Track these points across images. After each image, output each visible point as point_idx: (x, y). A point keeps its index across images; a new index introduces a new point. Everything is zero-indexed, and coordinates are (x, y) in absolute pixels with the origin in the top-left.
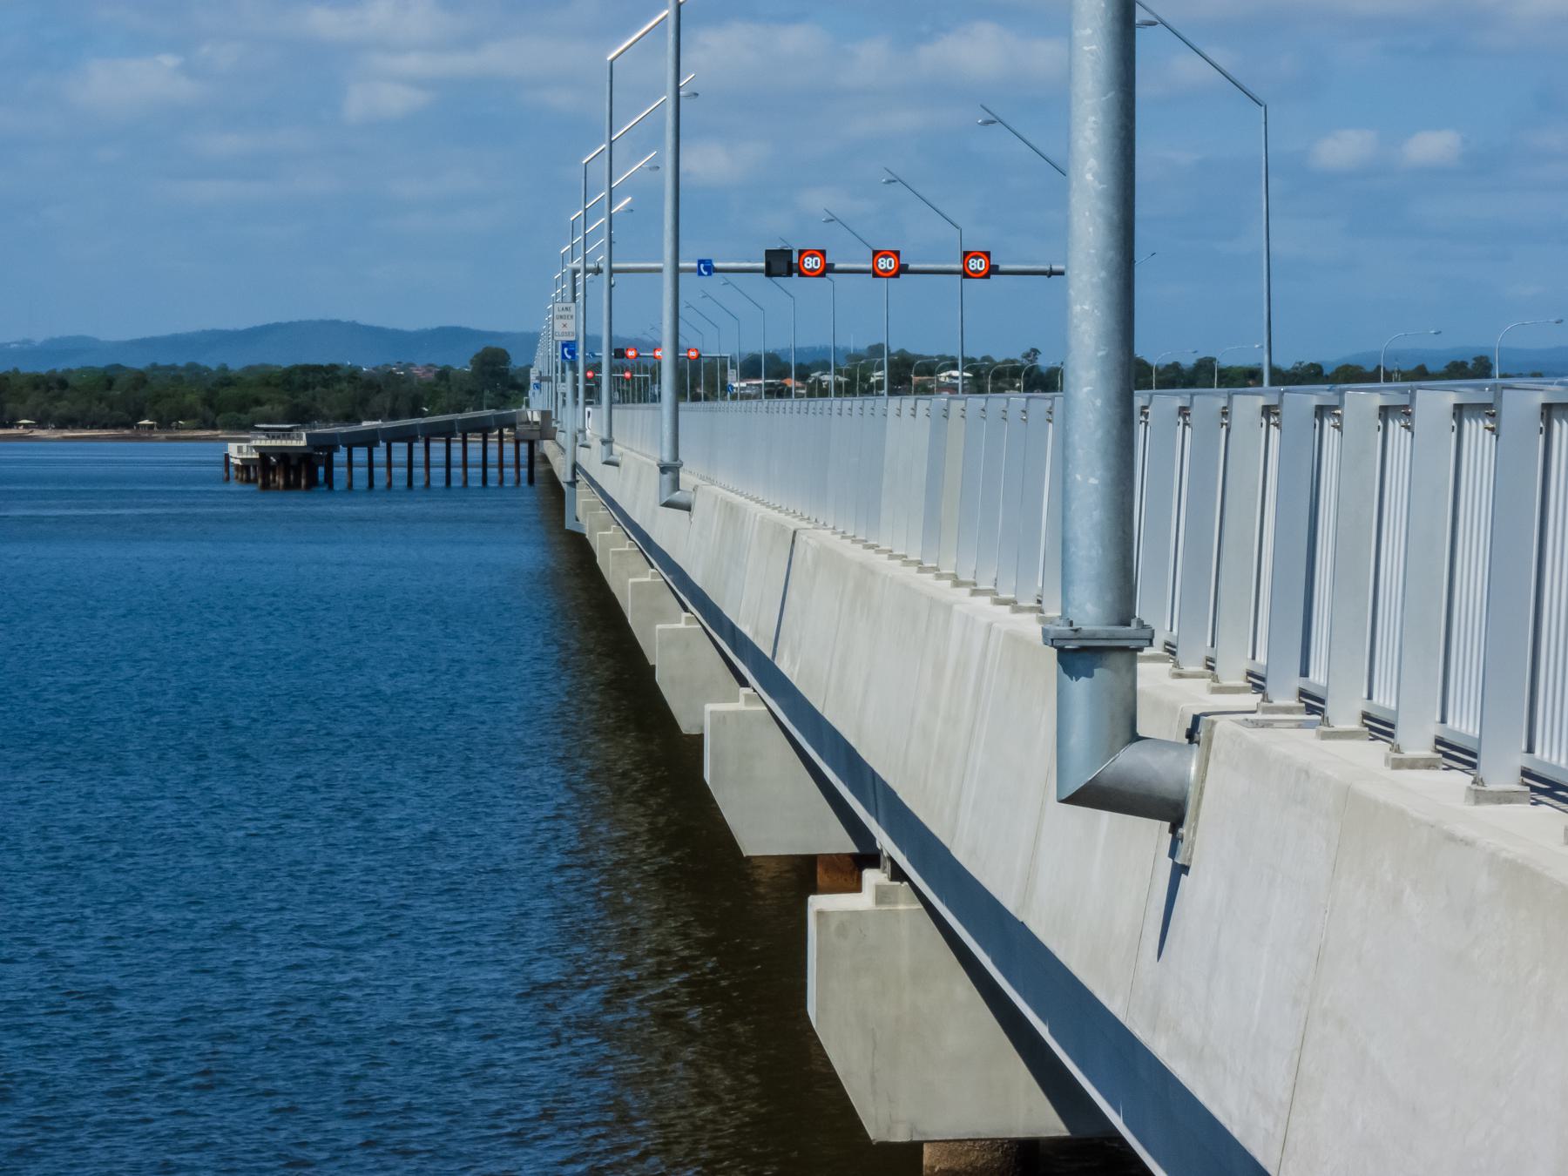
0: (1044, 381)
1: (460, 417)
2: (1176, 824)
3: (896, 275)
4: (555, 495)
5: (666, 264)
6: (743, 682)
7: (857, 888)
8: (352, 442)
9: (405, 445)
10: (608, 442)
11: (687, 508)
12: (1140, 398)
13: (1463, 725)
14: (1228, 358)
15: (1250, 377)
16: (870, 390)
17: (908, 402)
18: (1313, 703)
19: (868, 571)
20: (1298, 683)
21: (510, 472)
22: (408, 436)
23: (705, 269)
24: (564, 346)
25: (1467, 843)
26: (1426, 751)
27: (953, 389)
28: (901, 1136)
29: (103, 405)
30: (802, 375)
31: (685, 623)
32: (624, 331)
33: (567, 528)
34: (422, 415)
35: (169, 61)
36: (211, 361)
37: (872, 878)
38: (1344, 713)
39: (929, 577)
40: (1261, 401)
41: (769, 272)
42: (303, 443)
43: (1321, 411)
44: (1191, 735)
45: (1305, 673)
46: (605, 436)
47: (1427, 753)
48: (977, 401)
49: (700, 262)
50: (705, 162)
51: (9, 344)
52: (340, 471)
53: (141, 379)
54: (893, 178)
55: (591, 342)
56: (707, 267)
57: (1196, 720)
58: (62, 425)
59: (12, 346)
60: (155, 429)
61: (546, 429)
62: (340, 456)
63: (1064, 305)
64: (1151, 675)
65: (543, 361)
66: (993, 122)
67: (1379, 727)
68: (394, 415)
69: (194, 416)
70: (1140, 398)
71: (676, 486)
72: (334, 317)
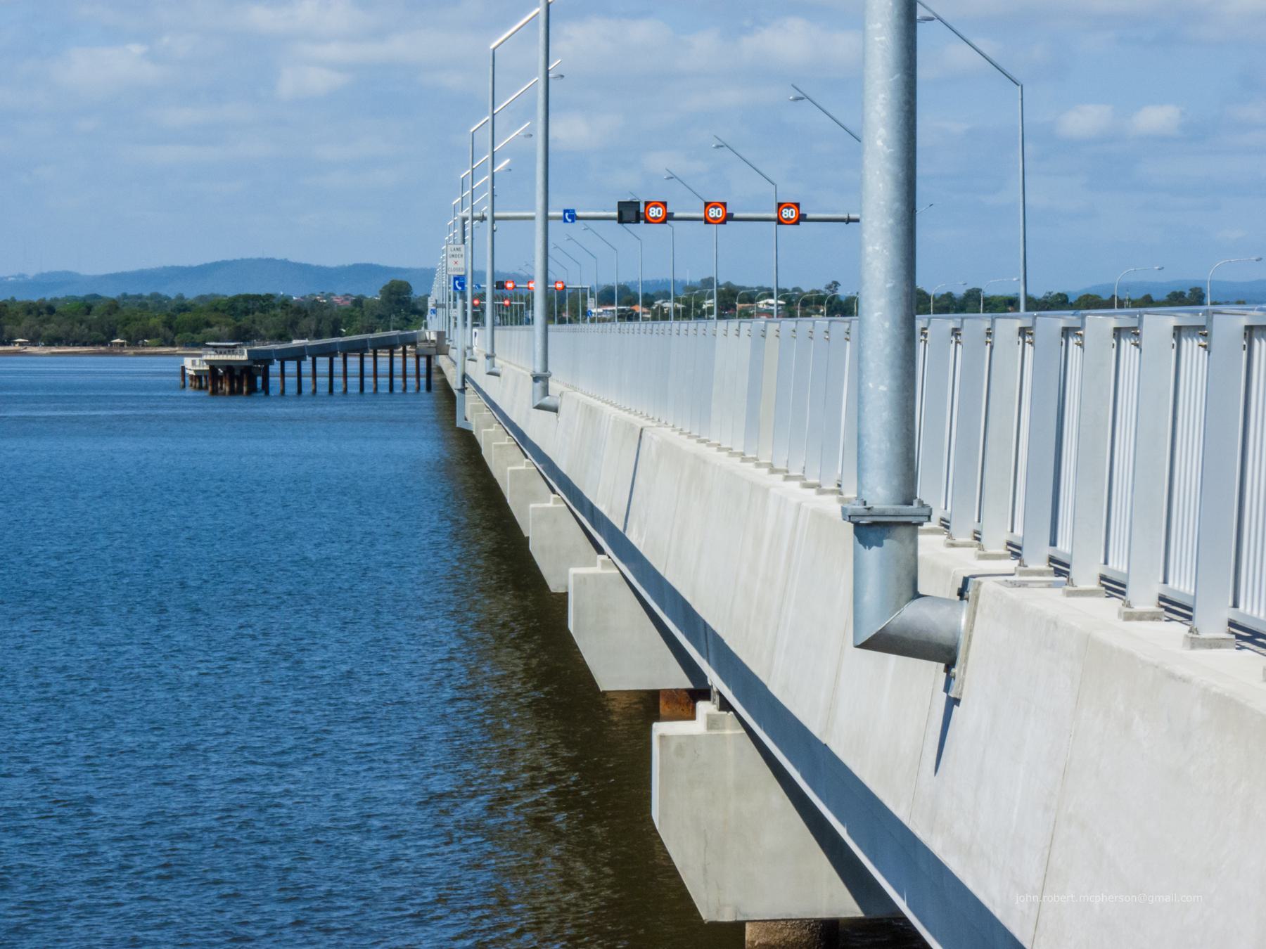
1: (371, 336)
2: (950, 665)
3: (724, 222)
4: (448, 399)
7: (692, 717)
8: (284, 357)
9: (327, 359)
12: (921, 321)
16: (702, 315)
17: (733, 324)
18: (1060, 568)
23: (569, 217)
24: (455, 279)
28: (727, 917)
29: (83, 327)
30: (648, 301)
31: (554, 503)
34: (340, 335)
36: (171, 291)
37: (705, 708)
41: (621, 220)
42: (245, 357)
43: (1067, 332)
44: (962, 593)
48: (789, 324)
49: (565, 211)
51: (7, 278)
53: (114, 306)
56: (571, 216)
59: (10, 279)
60: (125, 346)
61: (441, 346)
64: (929, 544)
65: (438, 292)
67: (1114, 587)
68: (318, 335)
69: (157, 336)
71: (546, 392)
72: (270, 256)
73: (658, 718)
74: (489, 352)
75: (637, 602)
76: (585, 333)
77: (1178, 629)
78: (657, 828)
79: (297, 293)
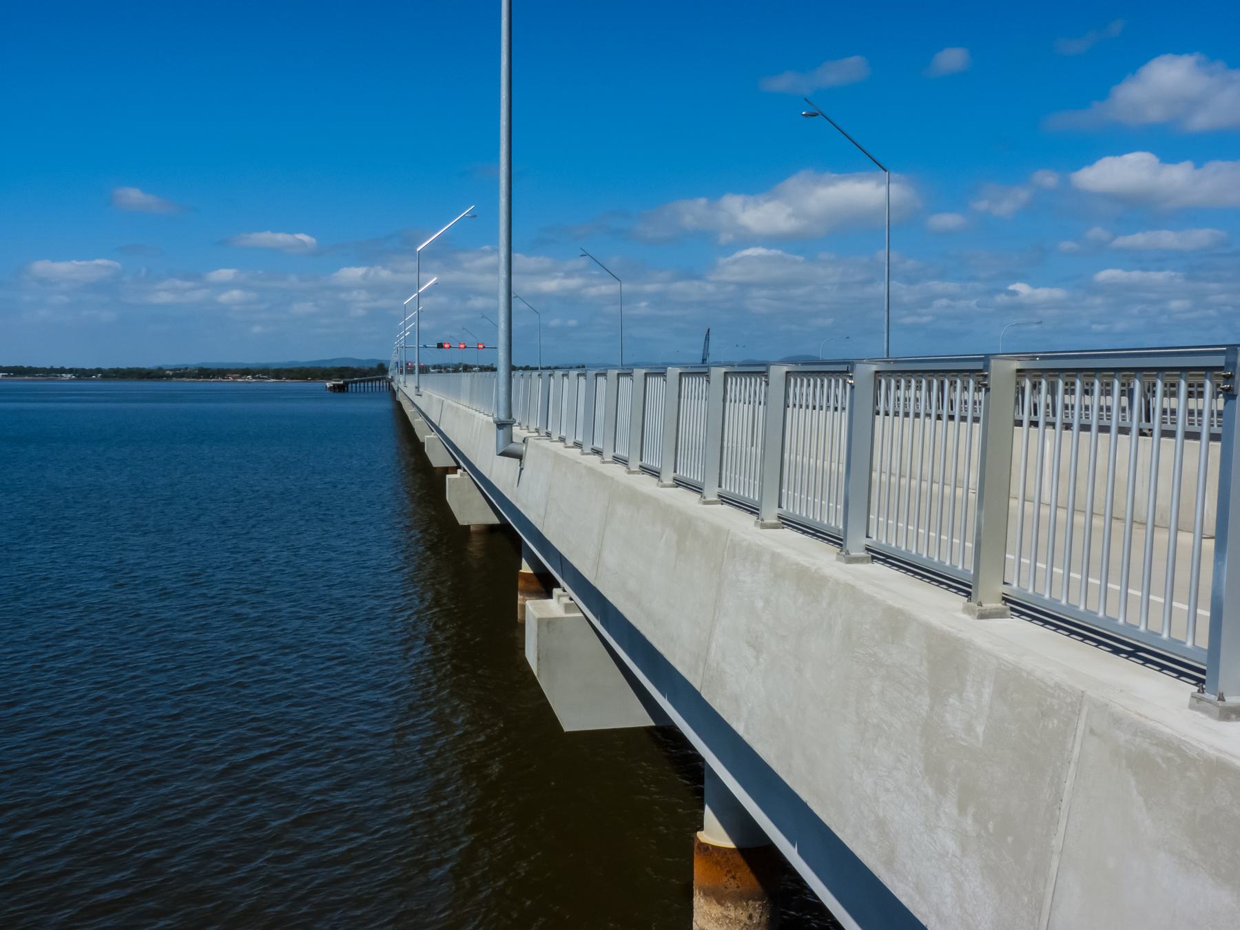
0: (494, 370)
2: (521, 460)
4: (394, 393)
5: (416, 346)
6: (433, 431)
8: (352, 382)
10: (405, 382)
11: (421, 396)
12: (513, 373)
13: (579, 439)
14: (531, 366)
15: (537, 369)
17: (466, 374)
18: (548, 435)
19: (458, 409)
20: (639, 463)
21: (385, 388)
22: (364, 381)
25: (580, 463)
26: (572, 445)
27: (475, 371)
28: (466, 524)
30: (445, 368)
31: (421, 419)
32: (408, 360)
33: (566, 729)
35: (310, 304)
36: (323, 366)
37: (459, 471)
38: (555, 437)
39: (470, 410)
40: (538, 373)
41: (438, 347)
43: (550, 375)
44: (524, 441)
45: (547, 428)
46: (417, 385)
47: (572, 445)
48: (480, 374)
50: (423, 325)
52: (350, 389)
54: (584, 253)
55: (401, 362)
57: (525, 439)
58: (292, 379)
61: (392, 380)
62: (350, 385)
63: (497, 354)
64: (516, 429)
65: (391, 366)
66: (815, 115)
67: (562, 440)
70: (513, 373)
71: (419, 391)
74: (503, 416)
79: (355, 366)
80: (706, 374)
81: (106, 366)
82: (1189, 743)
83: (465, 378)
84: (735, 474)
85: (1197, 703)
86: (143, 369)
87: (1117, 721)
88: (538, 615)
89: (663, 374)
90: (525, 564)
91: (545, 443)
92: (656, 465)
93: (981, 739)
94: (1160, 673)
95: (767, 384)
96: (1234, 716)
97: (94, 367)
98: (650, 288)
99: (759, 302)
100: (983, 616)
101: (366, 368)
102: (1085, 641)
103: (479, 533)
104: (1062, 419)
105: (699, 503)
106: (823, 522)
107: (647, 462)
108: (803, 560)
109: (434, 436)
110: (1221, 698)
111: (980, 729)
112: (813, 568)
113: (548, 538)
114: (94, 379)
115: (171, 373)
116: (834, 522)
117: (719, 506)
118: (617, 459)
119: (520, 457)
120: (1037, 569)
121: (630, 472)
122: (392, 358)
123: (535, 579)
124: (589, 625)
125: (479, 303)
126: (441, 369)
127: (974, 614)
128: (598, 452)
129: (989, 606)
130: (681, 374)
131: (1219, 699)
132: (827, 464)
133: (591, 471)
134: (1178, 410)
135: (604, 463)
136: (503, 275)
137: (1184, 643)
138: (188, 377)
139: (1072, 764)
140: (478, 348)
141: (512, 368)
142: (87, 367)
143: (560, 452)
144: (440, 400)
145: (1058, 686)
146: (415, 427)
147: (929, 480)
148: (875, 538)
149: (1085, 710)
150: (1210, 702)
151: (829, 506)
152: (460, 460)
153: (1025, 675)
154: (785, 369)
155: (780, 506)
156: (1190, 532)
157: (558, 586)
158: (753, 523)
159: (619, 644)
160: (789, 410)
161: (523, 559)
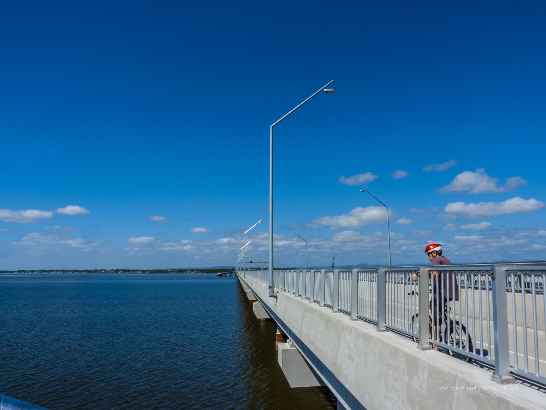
2: (276, 298)
4: (237, 277)
7: (256, 302)
8: (224, 273)
10: (241, 273)
12: (274, 271)
13: (294, 291)
16: (257, 270)
17: (259, 271)
18: (285, 290)
19: (257, 282)
26: (297, 295)
28: (259, 318)
30: (253, 269)
31: (245, 285)
32: (241, 266)
36: (215, 268)
37: (257, 301)
43: (285, 272)
44: (277, 292)
46: (271, 285)
47: (356, 318)
48: (264, 271)
53: (211, 270)
55: (239, 267)
56: (247, 262)
61: (237, 273)
64: (275, 288)
65: (236, 268)
67: (289, 292)
73: (254, 302)
74: (271, 285)
75: (307, 365)
76: (248, 272)
77: (289, 293)
78: (282, 368)
79: (225, 269)
80: (333, 271)
81: (151, 269)
82: (491, 392)
83: (259, 272)
84: (343, 302)
85: (493, 378)
86: (162, 270)
87: (468, 384)
88: (282, 348)
89: (320, 271)
90: (278, 331)
91: (284, 293)
92: (318, 300)
93: (425, 391)
94: (529, 388)
95: (352, 274)
96: (505, 383)
97: (147, 269)
98: (313, 243)
99: (349, 248)
100: (423, 349)
101: (139, 238)
102: (489, 370)
103: (263, 321)
104: (467, 285)
105: (332, 312)
106: (396, 327)
107: (315, 299)
108: (365, 331)
109: (249, 290)
110: (501, 377)
111: (424, 387)
112: (369, 333)
113: (285, 323)
114: (147, 273)
115: (170, 271)
116: (375, 319)
117: (338, 313)
118: (306, 298)
119: (276, 297)
120: (483, 346)
121: (310, 302)
122: (237, 266)
123: (281, 336)
124: (299, 353)
125: (262, 249)
126: (251, 269)
127: (420, 348)
128: (300, 296)
129: (425, 346)
130: (325, 271)
131: (500, 377)
132: (363, 297)
133: (298, 302)
134: (543, 283)
135: (302, 299)
136: (271, 241)
137: (535, 375)
138: (175, 272)
139: (455, 400)
140: (263, 263)
141: (274, 269)
142: (145, 269)
143: (288, 296)
144: (251, 279)
145: (448, 373)
146: (243, 287)
147: (415, 305)
148: (388, 324)
149: (458, 381)
150: (497, 378)
151: (398, 320)
152: (258, 298)
153: (437, 369)
154: (357, 270)
155: (357, 313)
156: (543, 331)
157: (288, 339)
158: (349, 319)
159: (308, 358)
160: (359, 281)
161: (277, 330)
